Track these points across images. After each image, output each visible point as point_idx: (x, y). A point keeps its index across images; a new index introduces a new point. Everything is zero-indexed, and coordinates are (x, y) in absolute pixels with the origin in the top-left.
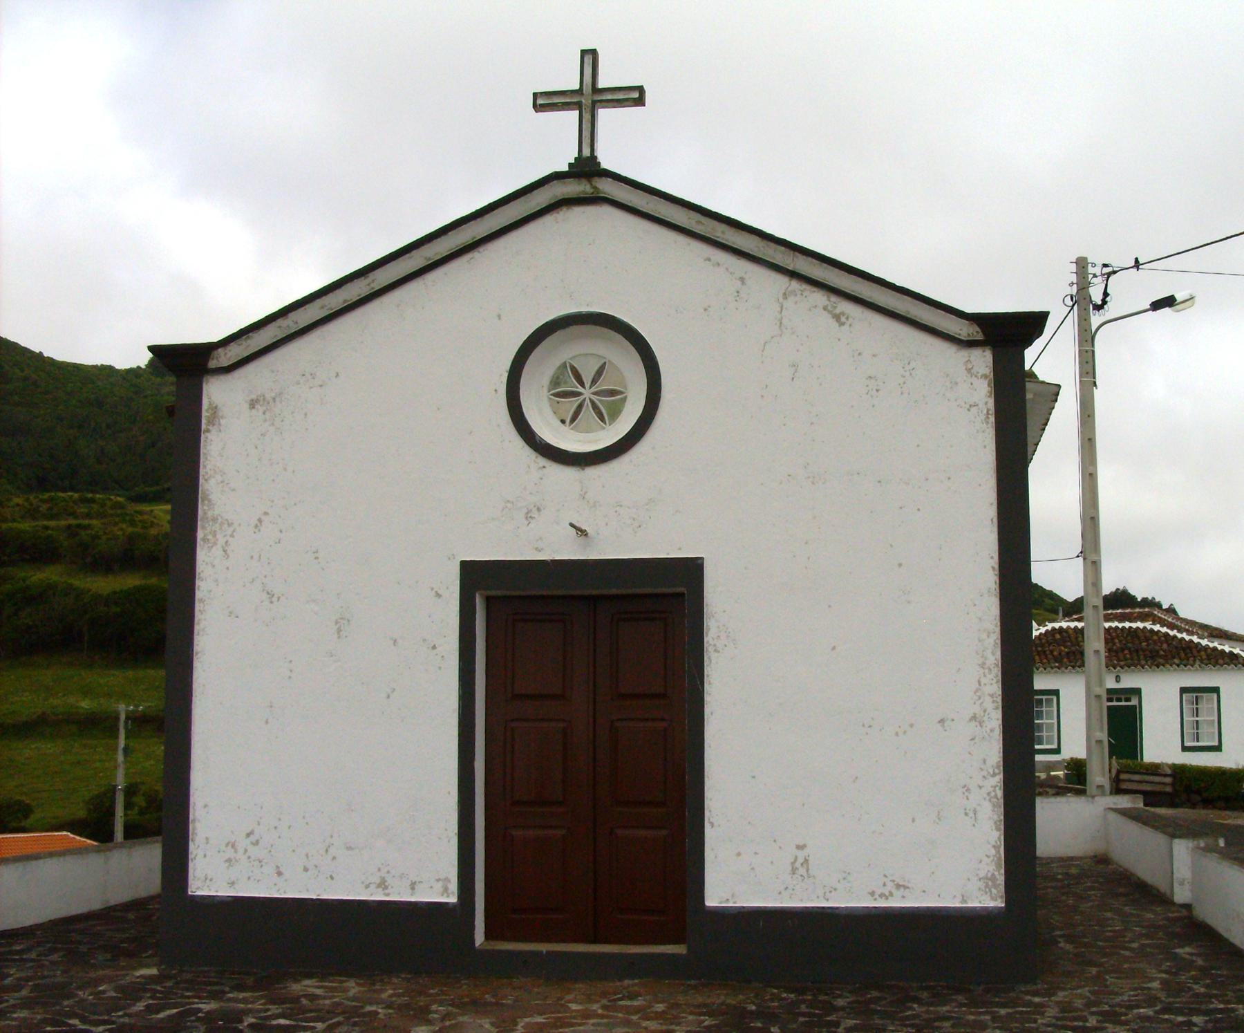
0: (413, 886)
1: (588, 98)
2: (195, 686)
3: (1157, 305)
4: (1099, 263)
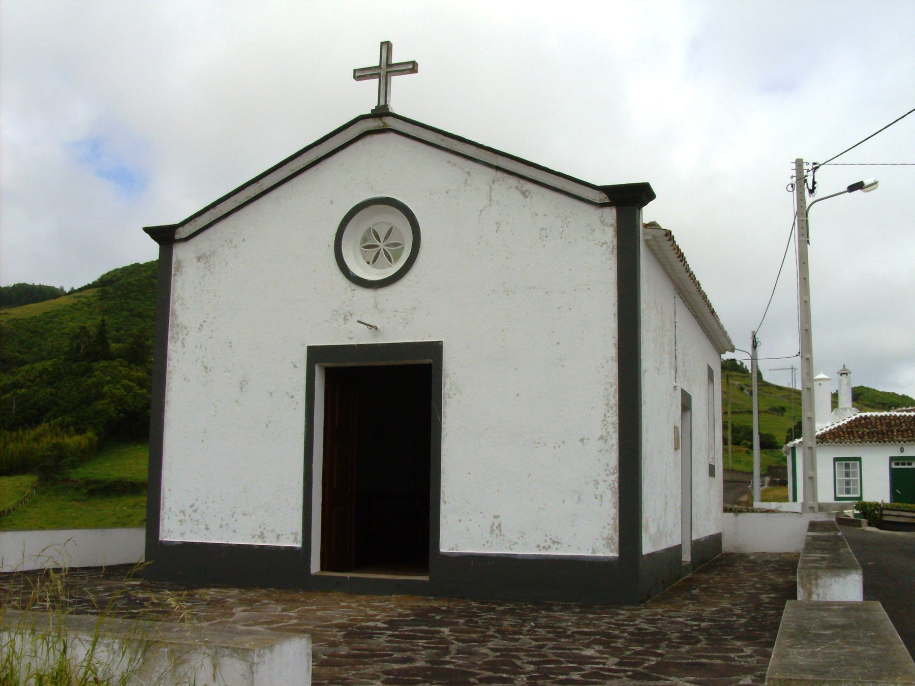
0: (278, 537)
1: (386, 69)
2: (165, 421)
3: (852, 188)
4: (811, 162)
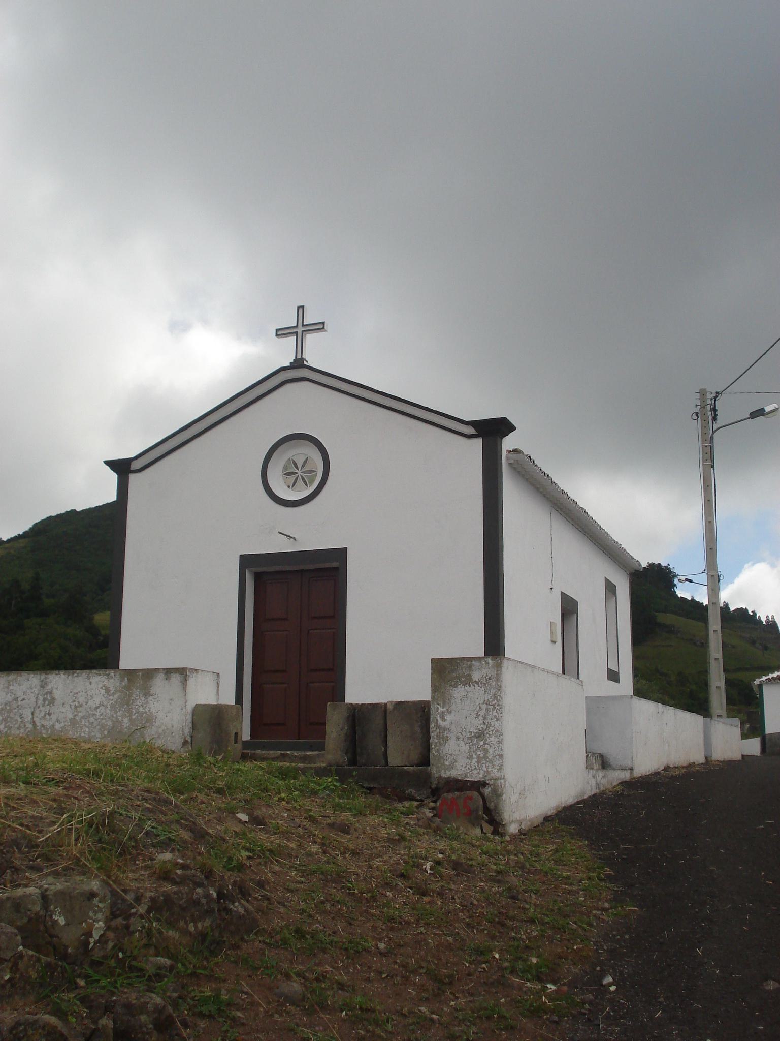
3: (755, 415)
